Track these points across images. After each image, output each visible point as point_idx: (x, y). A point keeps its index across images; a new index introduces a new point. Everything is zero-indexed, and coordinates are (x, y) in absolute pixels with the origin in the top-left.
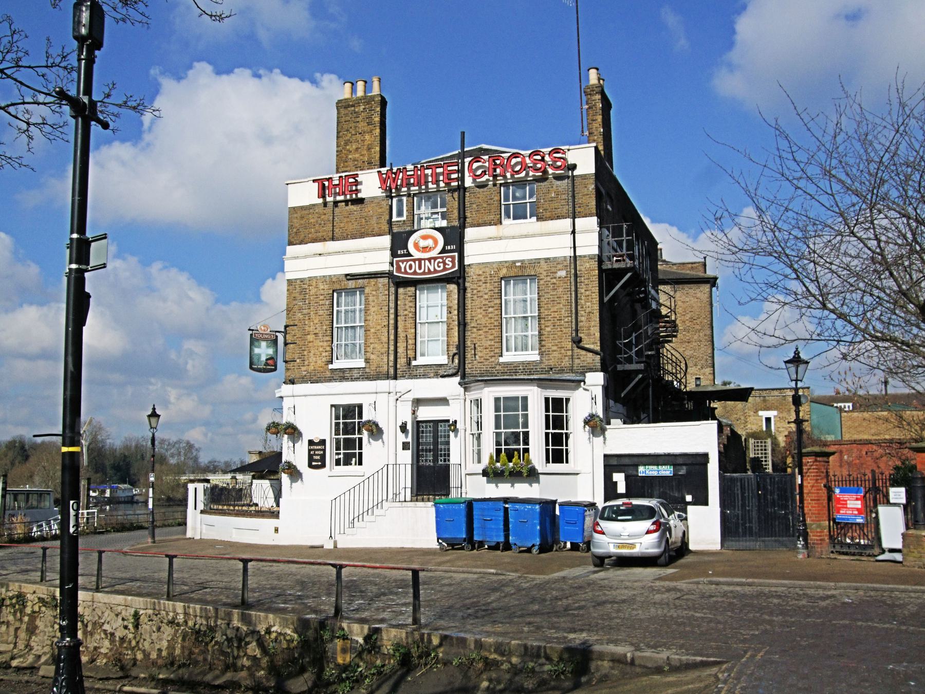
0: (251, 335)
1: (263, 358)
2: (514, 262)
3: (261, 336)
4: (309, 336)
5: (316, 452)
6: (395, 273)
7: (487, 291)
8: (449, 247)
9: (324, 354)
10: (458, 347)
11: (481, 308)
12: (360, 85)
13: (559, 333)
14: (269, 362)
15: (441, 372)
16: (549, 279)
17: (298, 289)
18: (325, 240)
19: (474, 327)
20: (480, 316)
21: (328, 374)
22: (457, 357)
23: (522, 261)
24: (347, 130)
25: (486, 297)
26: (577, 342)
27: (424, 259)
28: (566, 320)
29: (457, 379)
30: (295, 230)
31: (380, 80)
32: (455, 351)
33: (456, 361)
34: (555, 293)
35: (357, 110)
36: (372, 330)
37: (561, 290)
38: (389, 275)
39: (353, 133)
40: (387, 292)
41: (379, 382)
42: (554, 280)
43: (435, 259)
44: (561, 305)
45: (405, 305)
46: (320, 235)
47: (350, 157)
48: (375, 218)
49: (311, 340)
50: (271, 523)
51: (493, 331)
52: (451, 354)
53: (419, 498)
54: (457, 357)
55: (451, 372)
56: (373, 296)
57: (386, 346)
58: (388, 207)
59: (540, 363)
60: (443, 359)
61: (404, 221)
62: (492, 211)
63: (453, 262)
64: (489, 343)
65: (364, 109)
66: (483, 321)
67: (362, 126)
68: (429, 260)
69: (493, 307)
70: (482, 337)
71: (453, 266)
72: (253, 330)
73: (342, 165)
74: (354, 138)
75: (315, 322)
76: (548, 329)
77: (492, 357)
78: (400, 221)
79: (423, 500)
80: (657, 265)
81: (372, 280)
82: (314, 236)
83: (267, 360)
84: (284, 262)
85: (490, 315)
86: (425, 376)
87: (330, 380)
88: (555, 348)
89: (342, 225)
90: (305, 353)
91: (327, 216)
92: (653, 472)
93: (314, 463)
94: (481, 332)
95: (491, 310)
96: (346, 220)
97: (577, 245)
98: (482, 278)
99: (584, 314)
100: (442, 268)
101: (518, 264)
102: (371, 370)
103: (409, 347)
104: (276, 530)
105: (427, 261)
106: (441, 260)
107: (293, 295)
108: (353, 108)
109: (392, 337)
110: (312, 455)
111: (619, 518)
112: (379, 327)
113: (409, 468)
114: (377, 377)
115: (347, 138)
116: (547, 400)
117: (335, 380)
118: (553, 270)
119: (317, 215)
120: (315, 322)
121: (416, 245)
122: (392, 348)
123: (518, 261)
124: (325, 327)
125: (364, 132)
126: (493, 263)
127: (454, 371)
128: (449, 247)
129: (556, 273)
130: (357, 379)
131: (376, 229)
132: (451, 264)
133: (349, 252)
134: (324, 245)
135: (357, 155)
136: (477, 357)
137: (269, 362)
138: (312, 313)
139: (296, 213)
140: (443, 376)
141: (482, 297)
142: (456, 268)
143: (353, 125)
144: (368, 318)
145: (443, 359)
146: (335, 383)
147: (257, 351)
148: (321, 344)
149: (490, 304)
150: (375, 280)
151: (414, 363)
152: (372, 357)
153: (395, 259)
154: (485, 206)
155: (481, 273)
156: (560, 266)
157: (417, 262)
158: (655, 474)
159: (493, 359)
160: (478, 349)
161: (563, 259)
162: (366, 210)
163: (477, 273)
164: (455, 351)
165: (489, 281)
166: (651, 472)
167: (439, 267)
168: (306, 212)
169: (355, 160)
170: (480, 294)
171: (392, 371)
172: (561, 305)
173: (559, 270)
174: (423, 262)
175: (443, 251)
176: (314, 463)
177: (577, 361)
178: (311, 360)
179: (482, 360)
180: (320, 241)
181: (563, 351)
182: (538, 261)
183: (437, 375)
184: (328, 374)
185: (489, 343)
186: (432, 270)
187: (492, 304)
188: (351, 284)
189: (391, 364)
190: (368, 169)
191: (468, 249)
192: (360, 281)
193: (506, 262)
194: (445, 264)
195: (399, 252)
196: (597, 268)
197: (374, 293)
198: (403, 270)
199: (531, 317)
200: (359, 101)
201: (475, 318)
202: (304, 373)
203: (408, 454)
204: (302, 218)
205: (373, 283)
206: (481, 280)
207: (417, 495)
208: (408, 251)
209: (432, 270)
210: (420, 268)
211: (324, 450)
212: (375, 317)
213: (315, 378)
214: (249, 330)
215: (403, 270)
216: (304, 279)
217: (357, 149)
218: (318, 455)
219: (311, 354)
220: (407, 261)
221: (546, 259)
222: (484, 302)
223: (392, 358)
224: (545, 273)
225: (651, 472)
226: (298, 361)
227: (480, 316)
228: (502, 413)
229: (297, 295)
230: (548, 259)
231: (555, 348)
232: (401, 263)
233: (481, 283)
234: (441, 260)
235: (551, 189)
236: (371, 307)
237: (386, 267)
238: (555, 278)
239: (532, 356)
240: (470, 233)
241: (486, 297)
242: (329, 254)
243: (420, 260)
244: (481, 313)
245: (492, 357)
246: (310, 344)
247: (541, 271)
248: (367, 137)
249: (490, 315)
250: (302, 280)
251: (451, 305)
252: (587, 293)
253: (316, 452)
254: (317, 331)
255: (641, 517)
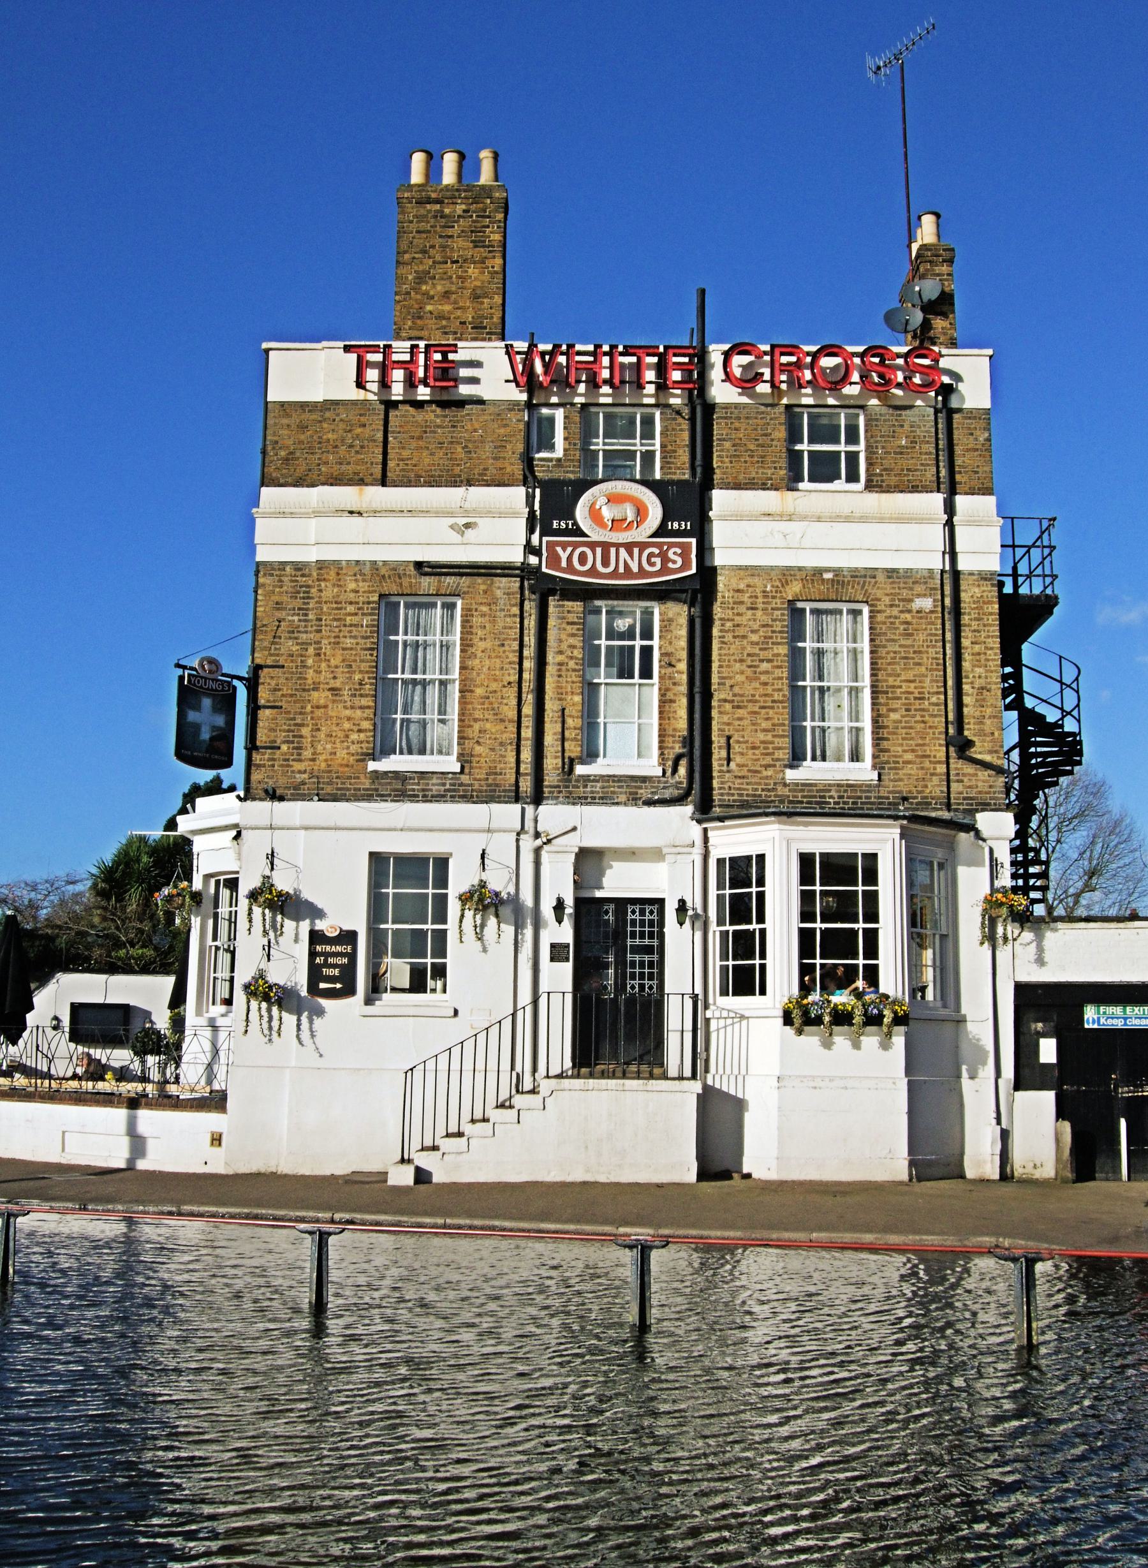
0: (181, 678)
1: (205, 735)
2: (818, 572)
3: (202, 682)
4: (315, 694)
5: (330, 960)
6: (544, 569)
7: (756, 627)
8: (676, 525)
9: (354, 736)
10: (688, 741)
11: (741, 661)
12: (450, 161)
13: (919, 726)
14: (217, 744)
15: (645, 793)
16: (895, 611)
17: (288, 585)
18: (361, 482)
19: (725, 701)
20: (740, 678)
21: (366, 783)
22: (683, 762)
23: (837, 571)
24: (424, 252)
25: (754, 638)
26: (961, 746)
27: (617, 546)
28: (934, 699)
29: (689, 809)
30: (283, 453)
31: (496, 157)
32: (678, 749)
33: (682, 771)
34: (909, 642)
35: (447, 211)
36: (479, 691)
37: (921, 636)
38: (525, 572)
39: (438, 258)
40: (516, 610)
41: (495, 807)
42: (908, 617)
43: (642, 546)
44: (923, 669)
45: (560, 641)
46: (350, 469)
47: (429, 308)
48: (489, 447)
49: (322, 702)
50: (210, 1121)
51: (771, 712)
52: (671, 755)
53: (583, 1070)
54: (683, 762)
55: (667, 794)
56: (483, 615)
57: (513, 728)
58: (522, 426)
59: (878, 786)
60: (651, 766)
61: (559, 460)
62: (769, 459)
63: (685, 555)
64: (761, 736)
65: (465, 211)
66: (749, 689)
67: (461, 246)
68: (629, 547)
69: (769, 661)
70: (746, 722)
71: (686, 565)
72: (184, 667)
73: (409, 323)
74: (440, 269)
75: (333, 662)
76: (894, 716)
77: (767, 767)
78: (550, 460)
79: (638, 1076)
80: (1031, 597)
81: (479, 580)
82: (336, 470)
83: (212, 739)
84: (252, 521)
85: (763, 678)
86: (606, 799)
87: (368, 796)
88: (909, 756)
89: (406, 453)
90: (305, 731)
91: (367, 430)
92: (1115, 1022)
93: (322, 986)
94: (741, 712)
95: (765, 666)
96: (414, 443)
97: (958, 548)
98: (745, 598)
99: (971, 691)
100: (658, 567)
101: (828, 576)
102: (477, 778)
103: (567, 734)
104: (217, 1140)
105: (622, 551)
106: (656, 551)
107: (276, 598)
108: (438, 207)
109: (528, 710)
110: (321, 966)
111: (186, 1208)
112: (494, 686)
113: (569, 998)
114: (490, 796)
115: (421, 268)
116: (763, 992)
117: (383, 798)
118: (905, 593)
119: (342, 426)
120: (333, 662)
121: (595, 515)
122: (528, 733)
123: (828, 570)
124: (357, 677)
125: (465, 261)
126: (772, 568)
127: (676, 793)
128: (676, 525)
129: (911, 601)
130: (439, 798)
131: (492, 471)
132: (679, 561)
133: (425, 513)
134: (361, 494)
135: (447, 308)
136: (733, 765)
137: (217, 744)
138: (324, 641)
139: (288, 416)
140: (650, 803)
141: (744, 637)
142: (694, 571)
143: (438, 241)
144: (469, 663)
145: (651, 766)
146: (383, 804)
147: (220, 721)
148: (348, 712)
149: (763, 655)
150: (488, 580)
151: (580, 770)
152: (478, 749)
153: (545, 539)
154: (752, 447)
155: (742, 586)
156: (919, 589)
157: (599, 550)
158: (1119, 1024)
159: (770, 772)
160: (736, 748)
161: (926, 574)
162: (469, 427)
163: (735, 586)
164: (678, 749)
165: (760, 606)
166: (1110, 1022)
167: (652, 564)
168: (315, 416)
169: (441, 317)
170: (740, 632)
171: (526, 785)
172: (923, 669)
173: (919, 596)
174: (613, 550)
175: (661, 531)
176: (322, 986)
177: (954, 787)
178: (319, 748)
179: (744, 773)
180: (350, 482)
181: (927, 764)
182: (871, 573)
183: (634, 800)
184: (366, 783)
185: (761, 736)
186: (635, 569)
187: (768, 654)
188: (427, 583)
189: (527, 767)
190: (475, 339)
191: (720, 533)
192: (449, 580)
193: (800, 569)
194: (665, 560)
195: (555, 524)
196: (996, 600)
197: (485, 609)
198: (564, 564)
199: (606, 684)
200: (451, 194)
201: (728, 683)
202: (300, 777)
203: (566, 969)
204: (303, 427)
205: (483, 587)
206: (742, 603)
207: (581, 1065)
208: (575, 523)
209: (635, 569)
210: (605, 563)
211: (353, 957)
212: (487, 662)
213: (329, 789)
214: (178, 666)
215: (564, 564)
216: (305, 565)
217: (447, 294)
218: (334, 966)
219: (322, 735)
220: (576, 545)
221: (887, 570)
222: (749, 649)
223: (527, 755)
224: (887, 600)
225: (1110, 1022)
226: (284, 747)
227: (740, 678)
228: (818, 888)
229: (285, 598)
230: (894, 570)
231: (909, 756)
232: (559, 549)
233: (742, 609)
234: (656, 551)
235: (898, 429)
236: (476, 640)
237: (516, 556)
238: (909, 611)
239: (864, 772)
240: (720, 498)
241: (754, 638)
242: (375, 513)
243: (606, 546)
244: (742, 673)
245: (767, 767)
246: (319, 713)
247: (879, 593)
248: (472, 271)
249: (763, 678)
250: (299, 567)
251: (670, 649)
252: (977, 648)
253: (330, 960)
254: (337, 684)
255: (957, 1128)
